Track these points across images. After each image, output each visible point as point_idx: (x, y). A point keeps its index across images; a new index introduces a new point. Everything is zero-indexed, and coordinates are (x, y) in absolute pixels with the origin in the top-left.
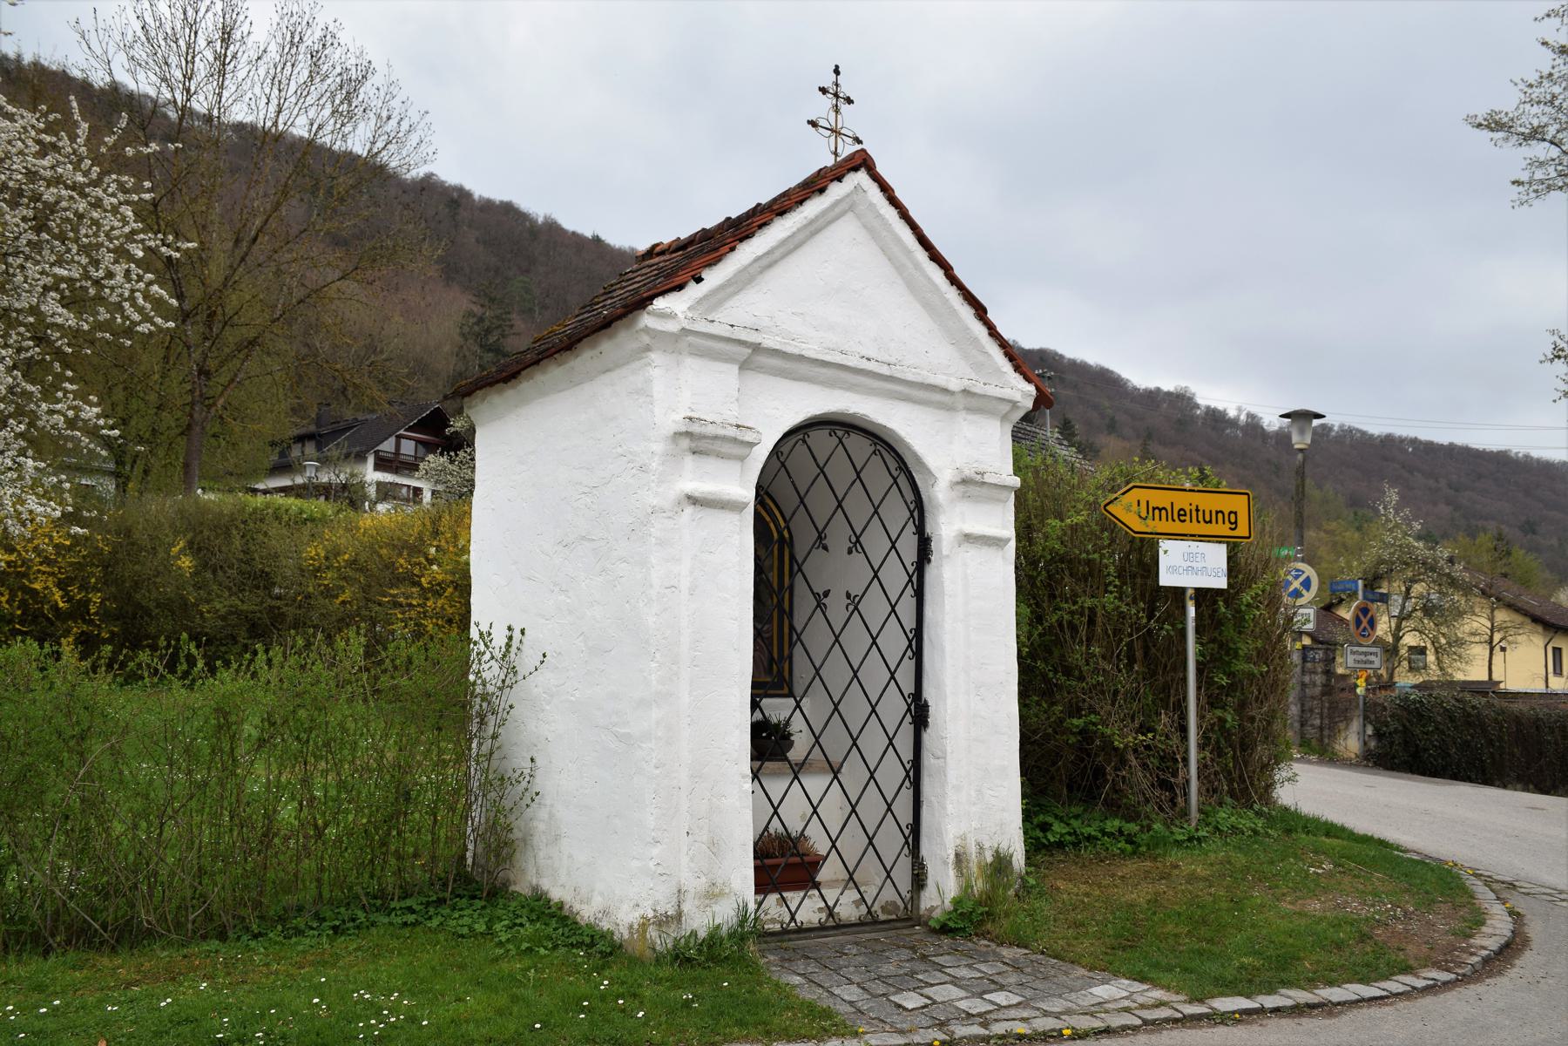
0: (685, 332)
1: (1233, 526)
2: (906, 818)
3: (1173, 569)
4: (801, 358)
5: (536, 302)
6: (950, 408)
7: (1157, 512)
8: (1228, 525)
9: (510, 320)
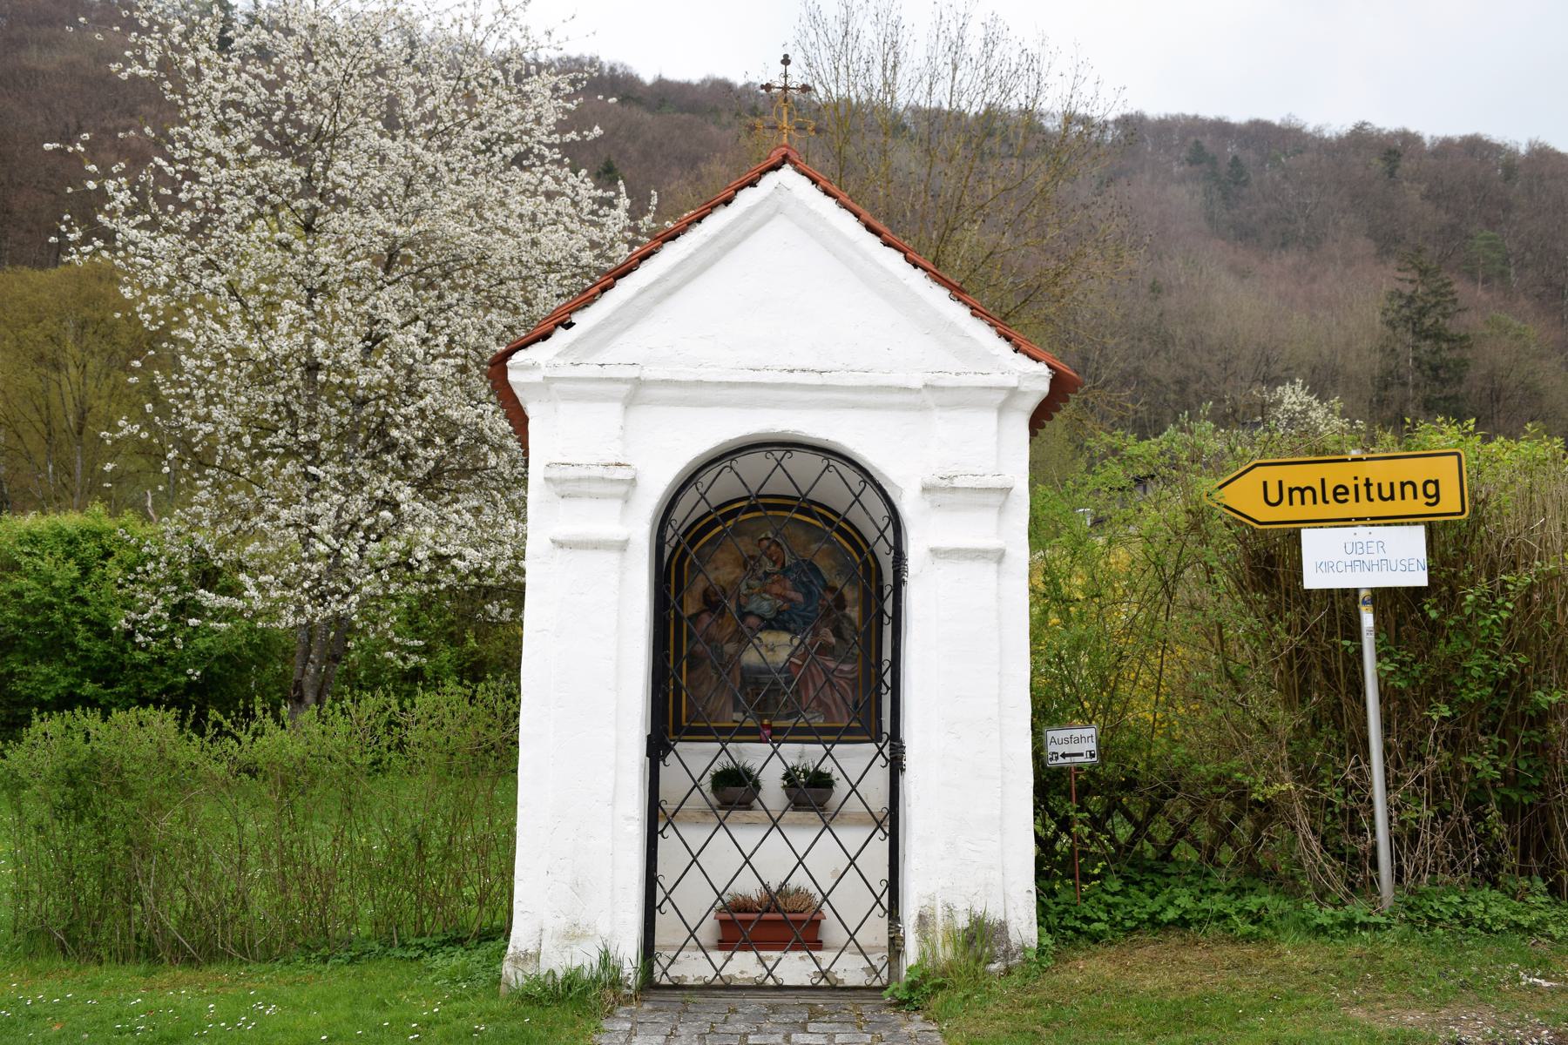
0: (549, 380)
1: (1433, 500)
2: (878, 871)
3: (1328, 566)
4: (700, 384)
5: (1512, 261)
6: (923, 408)
7: (1296, 494)
8: (1422, 498)
9: (1452, 293)
